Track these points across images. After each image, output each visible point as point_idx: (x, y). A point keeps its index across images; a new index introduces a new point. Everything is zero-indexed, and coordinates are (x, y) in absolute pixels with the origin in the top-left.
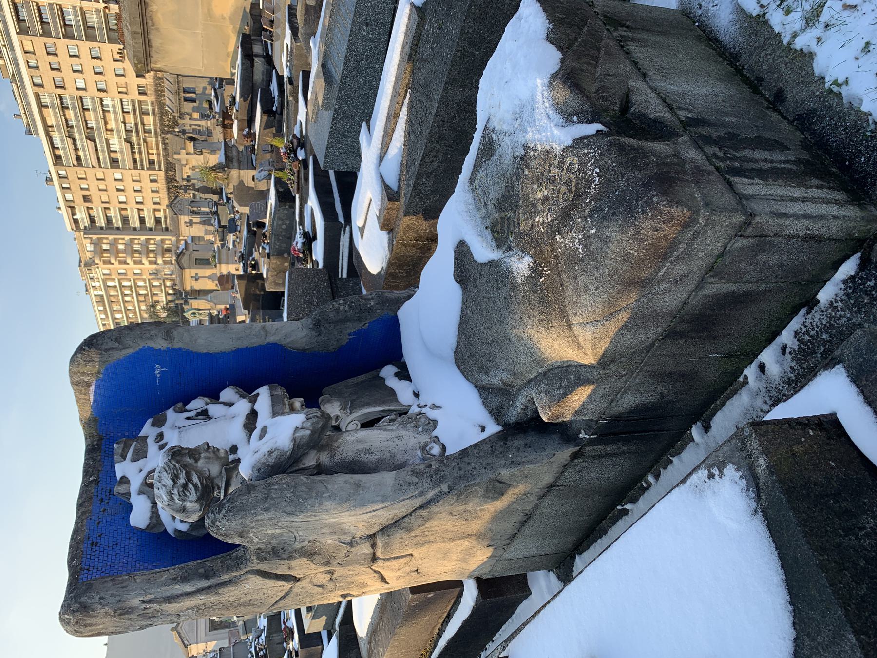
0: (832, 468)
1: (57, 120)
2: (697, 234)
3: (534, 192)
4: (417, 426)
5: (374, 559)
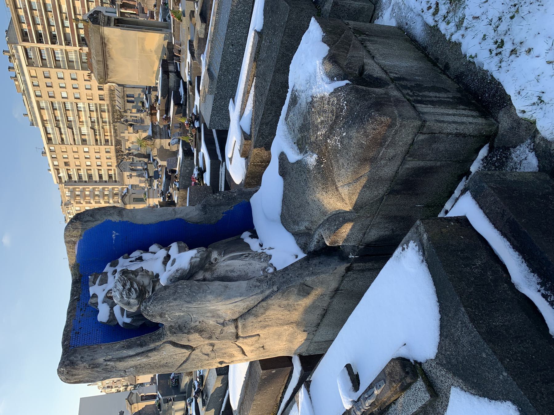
0: (462, 239)
1: (49, 117)
2: (396, 131)
3: (317, 120)
4: (260, 259)
5: (237, 337)
